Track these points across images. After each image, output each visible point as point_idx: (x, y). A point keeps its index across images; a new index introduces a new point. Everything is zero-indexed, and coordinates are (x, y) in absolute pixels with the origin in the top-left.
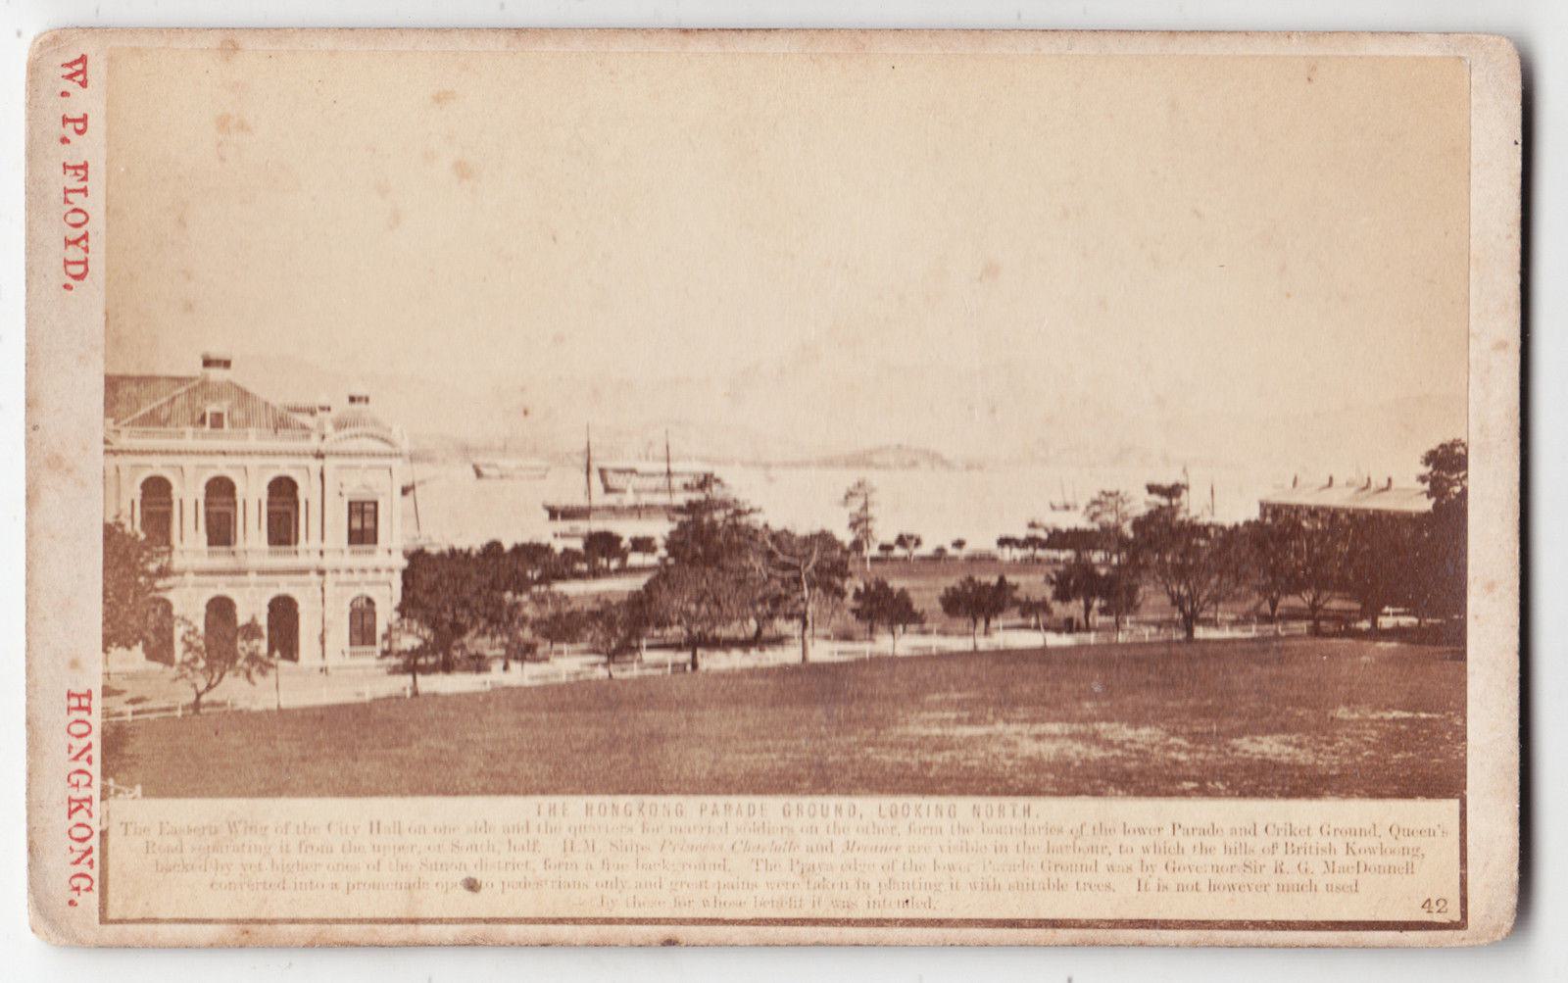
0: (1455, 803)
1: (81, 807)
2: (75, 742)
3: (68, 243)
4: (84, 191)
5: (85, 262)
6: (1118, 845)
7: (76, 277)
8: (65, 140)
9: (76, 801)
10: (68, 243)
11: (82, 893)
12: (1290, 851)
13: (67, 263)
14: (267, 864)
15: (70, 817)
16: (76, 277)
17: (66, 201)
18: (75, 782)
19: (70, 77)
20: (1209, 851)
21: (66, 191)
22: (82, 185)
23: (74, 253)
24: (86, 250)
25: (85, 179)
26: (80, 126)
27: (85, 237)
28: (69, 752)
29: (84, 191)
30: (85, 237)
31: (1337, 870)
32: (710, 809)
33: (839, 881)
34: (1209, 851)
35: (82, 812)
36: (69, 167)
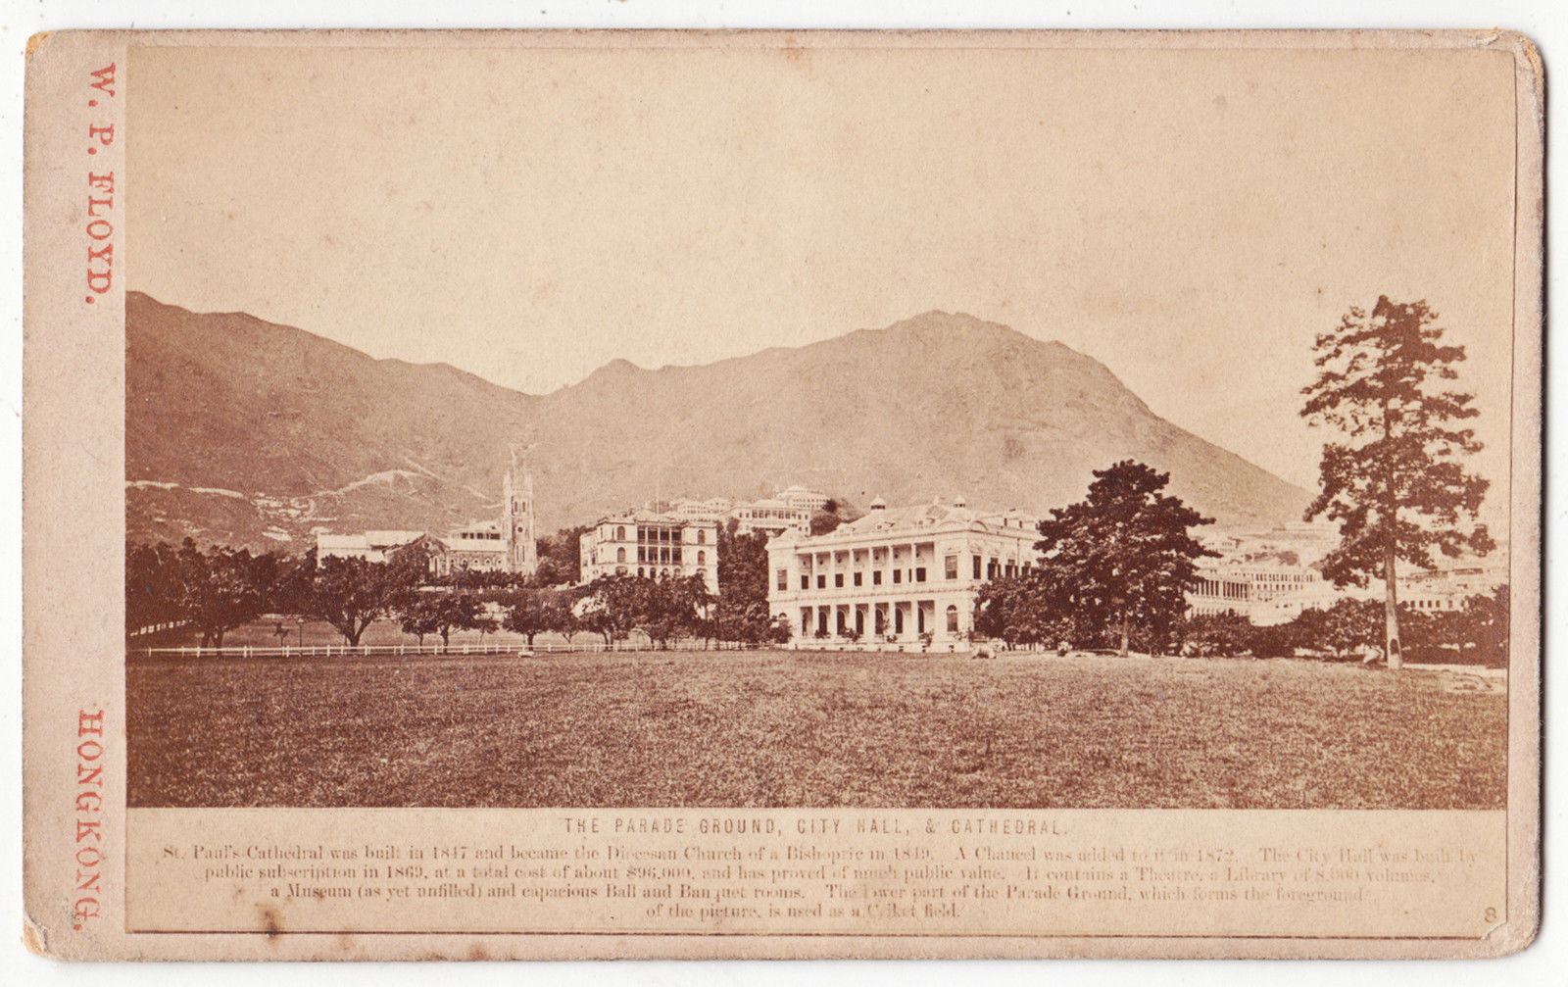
0: (1505, 671)
1: (89, 831)
2: (86, 764)
3: (92, 255)
4: (109, 203)
5: (108, 275)
6: (1214, 516)
7: (100, 291)
8: (92, 151)
9: (85, 824)
10: (92, 255)
11: (58, 920)
12: (686, 894)
13: (91, 275)
14: (735, 870)
15: (78, 840)
16: (100, 291)
17: (91, 212)
18: (84, 805)
19: (99, 86)
20: (686, 913)
21: (92, 202)
22: (107, 196)
23: (99, 266)
24: (109, 261)
25: (111, 190)
26: (107, 136)
27: (109, 250)
28: (79, 774)
29: (109, 203)
30: (109, 250)
31: (301, 892)
32: (626, 824)
33: (482, 898)
34: (686, 913)
35: (91, 836)
36: (97, 178)
